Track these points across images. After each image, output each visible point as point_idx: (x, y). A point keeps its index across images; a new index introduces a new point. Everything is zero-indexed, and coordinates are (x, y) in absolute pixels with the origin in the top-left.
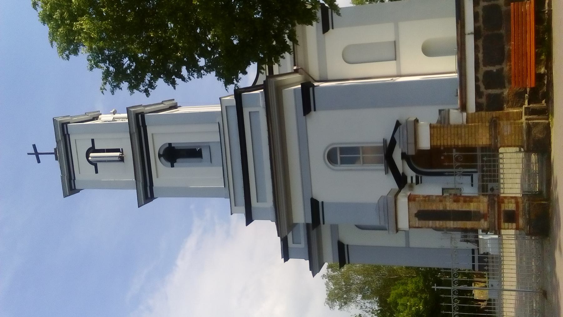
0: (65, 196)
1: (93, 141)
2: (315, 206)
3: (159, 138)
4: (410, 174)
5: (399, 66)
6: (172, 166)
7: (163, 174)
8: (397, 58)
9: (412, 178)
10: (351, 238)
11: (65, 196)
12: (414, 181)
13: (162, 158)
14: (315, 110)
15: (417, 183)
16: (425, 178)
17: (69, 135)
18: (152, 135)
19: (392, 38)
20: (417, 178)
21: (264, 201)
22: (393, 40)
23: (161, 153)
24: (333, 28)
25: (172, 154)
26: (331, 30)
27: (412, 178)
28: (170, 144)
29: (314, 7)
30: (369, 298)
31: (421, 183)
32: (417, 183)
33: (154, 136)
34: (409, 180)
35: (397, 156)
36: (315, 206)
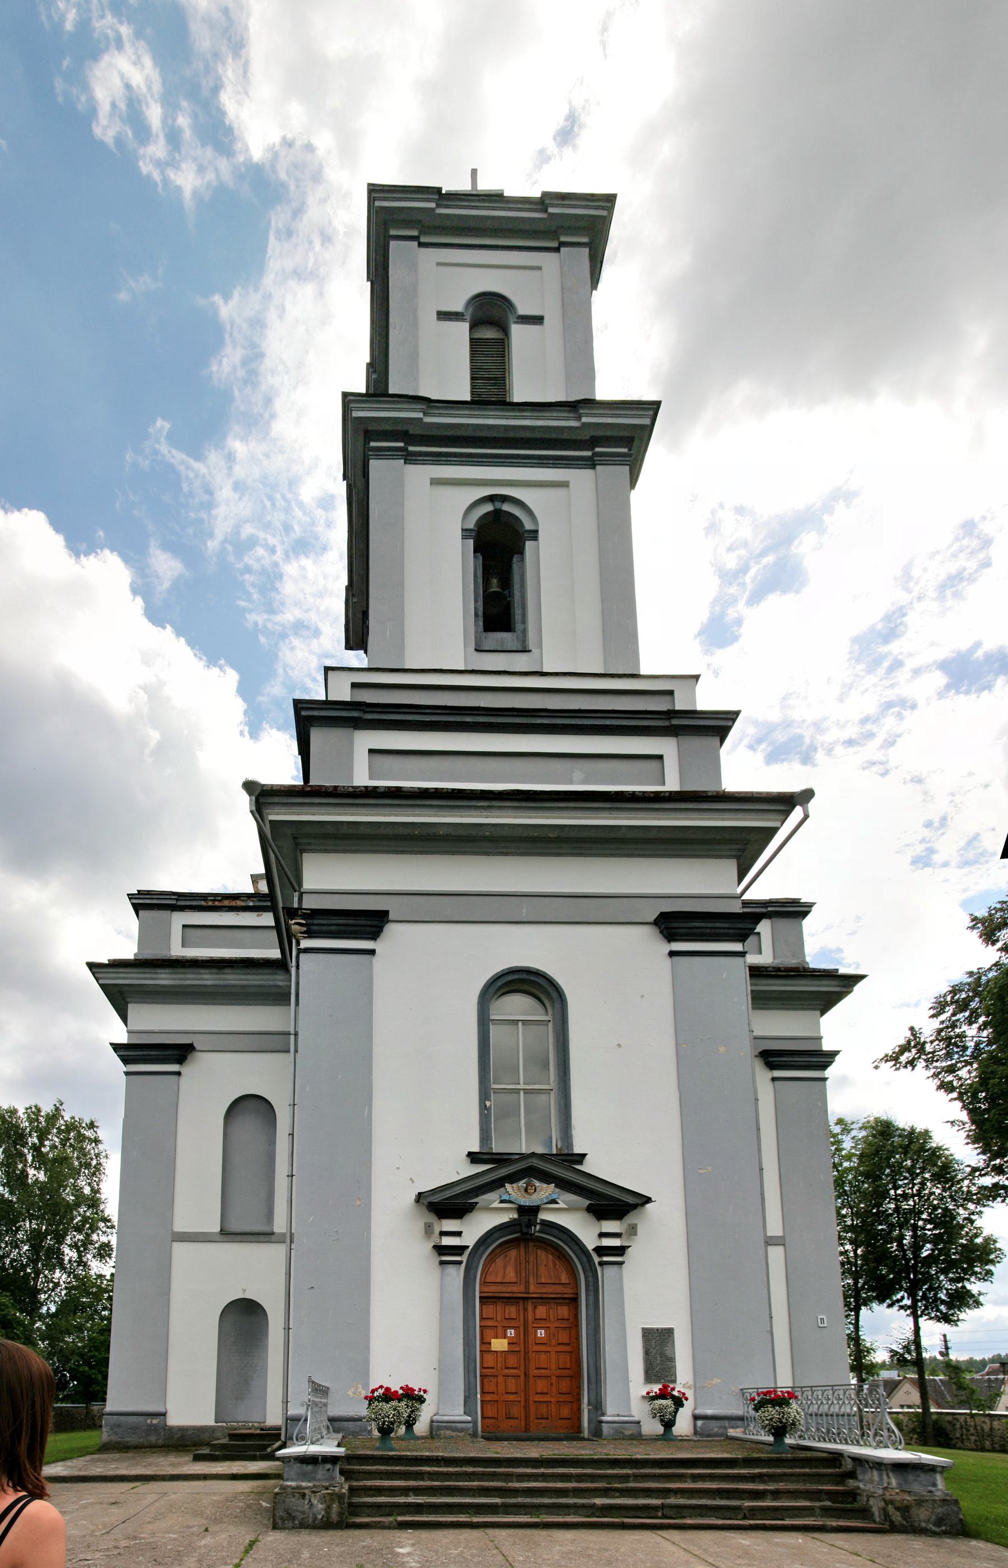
2: (367, 923)
3: (555, 502)
4: (472, 1230)
7: (434, 510)
8: (225, 1238)
9: (458, 1234)
10: (209, 1087)
12: (447, 1241)
15: (441, 1250)
16: (456, 1276)
17: (557, 250)
18: (565, 485)
20: (459, 1250)
25: (499, 544)
27: (458, 1234)
28: (534, 535)
29: (79, 1229)
30: (219, 78)
31: (442, 1263)
32: (441, 1250)
33: (174, 1077)
36: (367, 923)
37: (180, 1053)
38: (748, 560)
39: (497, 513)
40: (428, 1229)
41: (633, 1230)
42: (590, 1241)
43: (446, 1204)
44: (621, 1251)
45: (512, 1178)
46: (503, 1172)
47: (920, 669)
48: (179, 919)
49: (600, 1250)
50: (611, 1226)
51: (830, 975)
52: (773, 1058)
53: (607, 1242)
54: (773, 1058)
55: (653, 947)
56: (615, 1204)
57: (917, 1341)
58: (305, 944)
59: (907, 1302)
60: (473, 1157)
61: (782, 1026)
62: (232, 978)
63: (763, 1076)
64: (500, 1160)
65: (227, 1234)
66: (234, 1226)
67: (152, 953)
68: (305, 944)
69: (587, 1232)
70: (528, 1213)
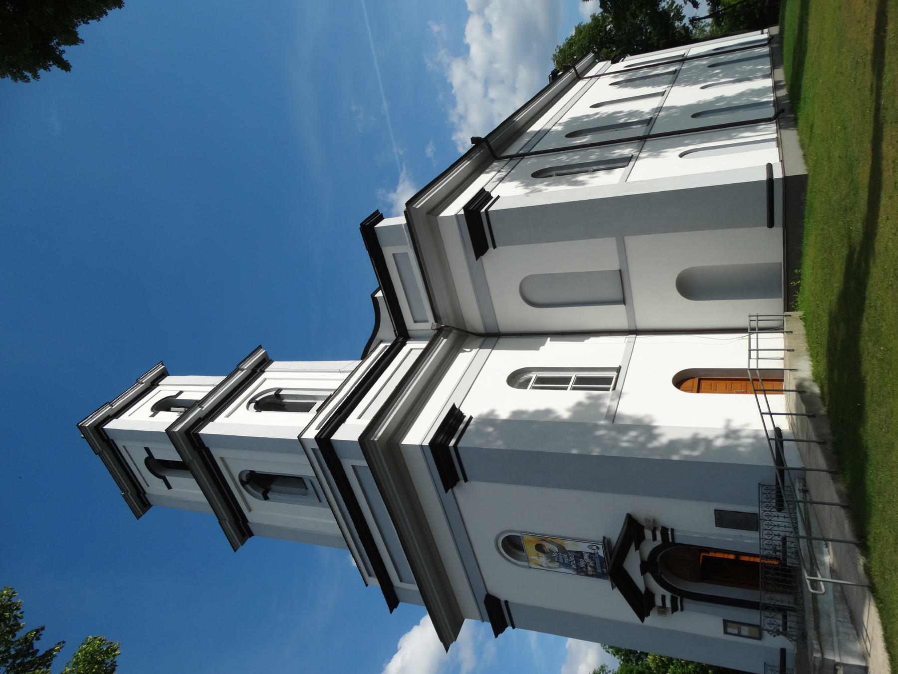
0: (138, 517)
1: (147, 449)
5: (631, 314)
6: (266, 498)
9: (663, 598)
11: (138, 517)
12: (668, 604)
13: (248, 486)
14: (466, 480)
15: (674, 609)
16: (688, 603)
19: (616, 266)
20: (674, 601)
21: (407, 587)
22: (617, 268)
23: (245, 480)
24: (466, 480)
26: (491, 248)
34: (658, 602)
35: (633, 564)
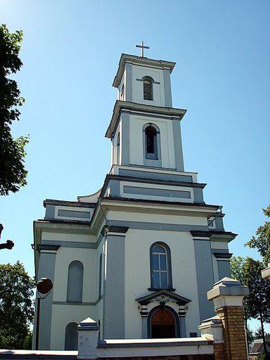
10: (64, 257)
12: (143, 311)
15: (142, 313)
20: (146, 313)
28: (159, 133)
37: (55, 247)
38: (205, 149)
39: (150, 126)
40: (139, 308)
41: (187, 308)
42: (177, 311)
43: (143, 301)
44: (184, 313)
45: (159, 295)
46: (158, 293)
47: (209, 344)
48: (57, 208)
49: (180, 313)
50: (182, 307)
51: (230, 233)
52: (217, 255)
53: (181, 311)
54: (217, 255)
55: (190, 237)
56: (182, 302)
57: (263, 330)
58: (109, 233)
59: (259, 317)
60: (149, 290)
61: (217, 245)
62: (74, 227)
63: (214, 259)
64: (158, 290)
65: (69, 302)
66: (70, 300)
67: (50, 217)
68: (109, 233)
69: (176, 308)
70: (162, 303)
